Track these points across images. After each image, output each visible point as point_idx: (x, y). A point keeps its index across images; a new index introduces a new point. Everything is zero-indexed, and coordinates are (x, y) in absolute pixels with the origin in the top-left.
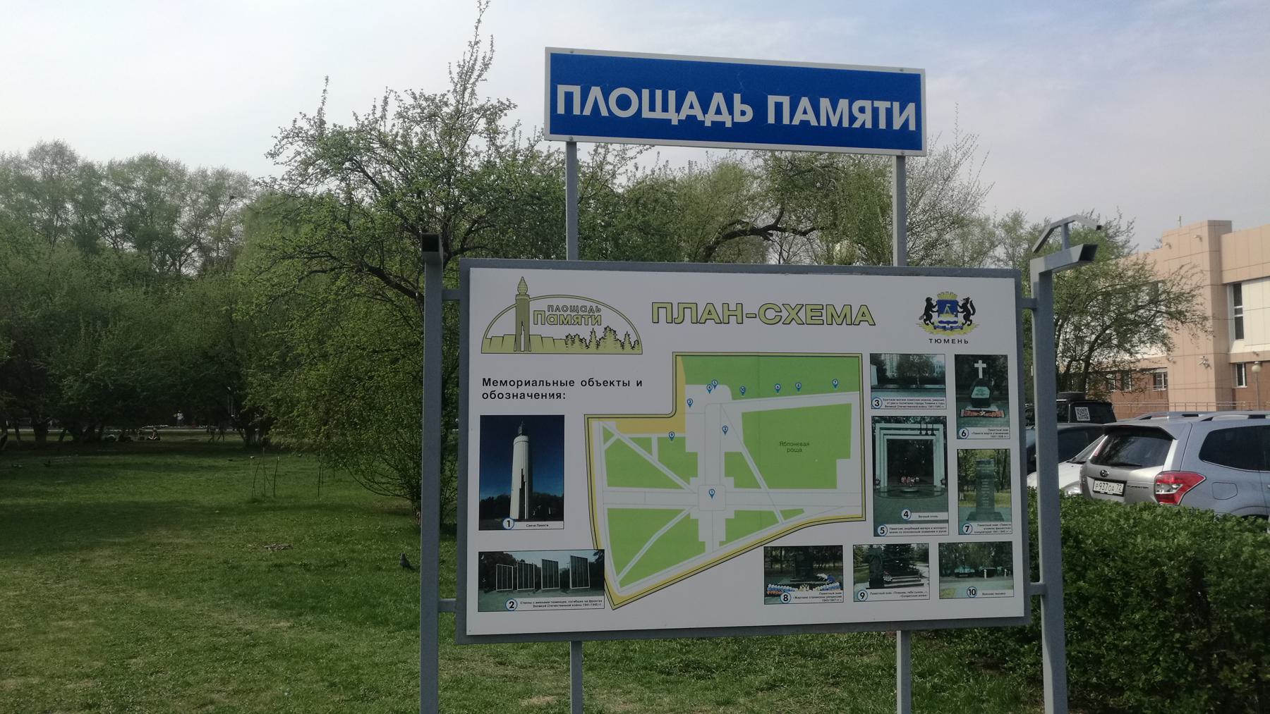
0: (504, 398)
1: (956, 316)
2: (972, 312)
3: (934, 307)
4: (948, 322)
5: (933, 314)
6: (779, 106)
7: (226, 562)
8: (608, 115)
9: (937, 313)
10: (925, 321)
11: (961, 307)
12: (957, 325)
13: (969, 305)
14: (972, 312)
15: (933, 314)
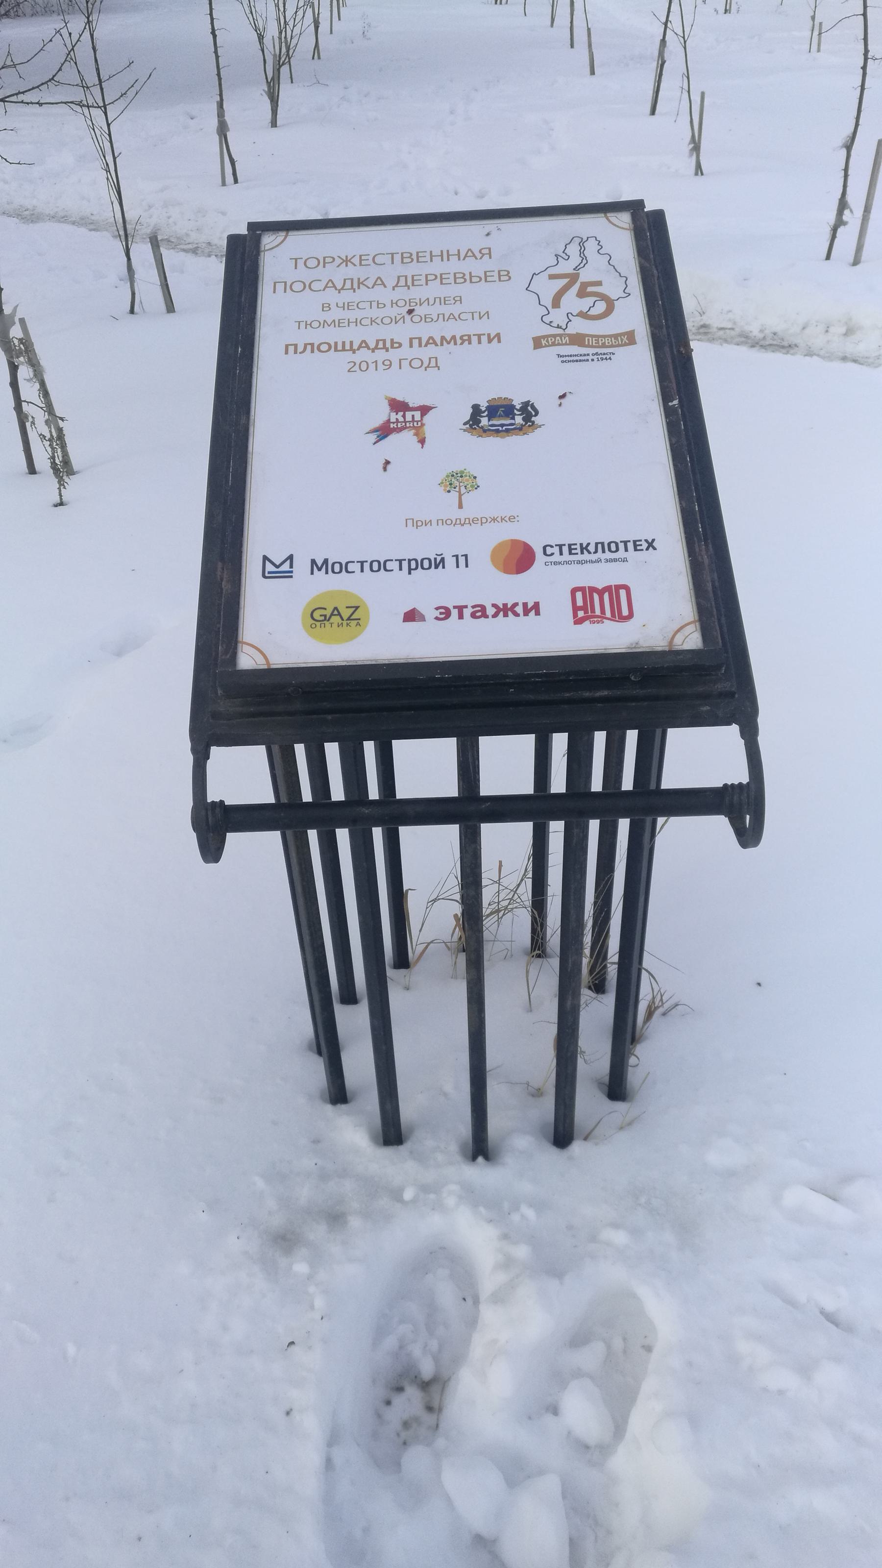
0: (371, 258)
1: (513, 418)
2: (534, 413)
3: (484, 412)
4: (502, 425)
5: (481, 419)
6: (588, 340)
7: (76, 115)
8: (587, 291)
9: (391, 421)
10: (471, 426)
11: (518, 410)
12: (515, 426)
13: (529, 408)
14: (534, 413)
15: (481, 419)
